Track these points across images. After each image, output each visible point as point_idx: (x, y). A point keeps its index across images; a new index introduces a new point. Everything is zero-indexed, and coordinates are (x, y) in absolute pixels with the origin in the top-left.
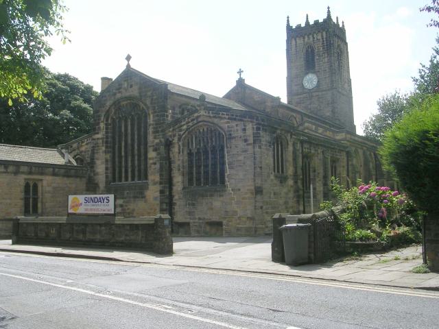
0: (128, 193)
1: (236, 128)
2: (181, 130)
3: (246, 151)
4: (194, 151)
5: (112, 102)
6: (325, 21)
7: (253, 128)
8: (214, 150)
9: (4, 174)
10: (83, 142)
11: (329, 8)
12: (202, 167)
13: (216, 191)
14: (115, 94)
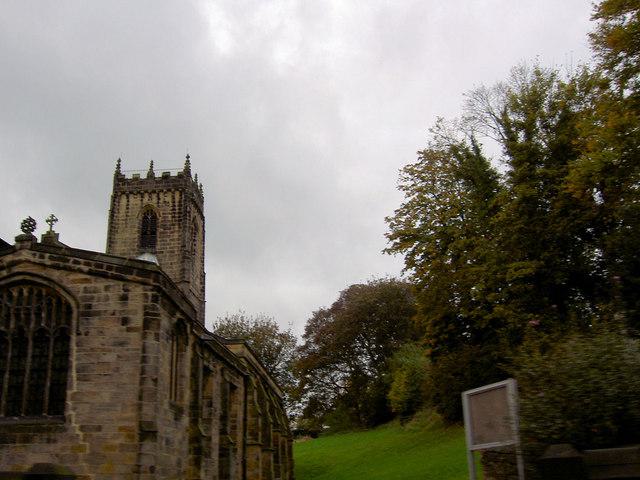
1: (104, 293)
6: (180, 176)
8: (41, 337)
11: (188, 157)
12: (7, 376)
13: (39, 430)
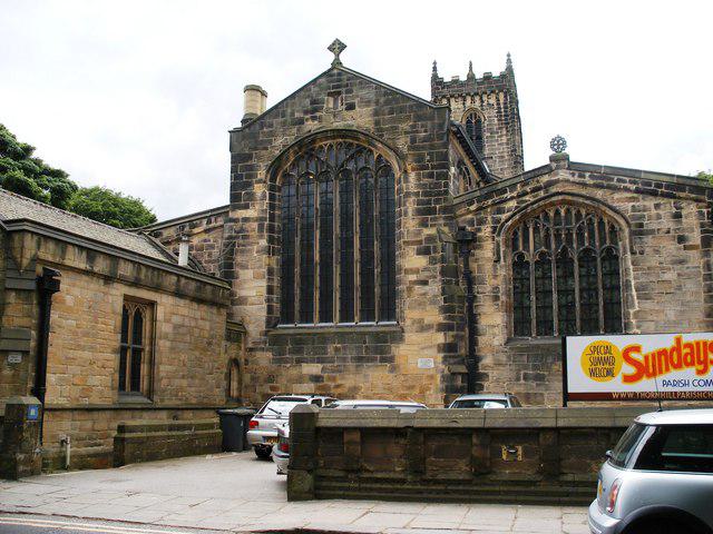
0: (337, 349)
1: (654, 212)
2: (500, 211)
3: (681, 262)
4: (531, 257)
5: (291, 140)
6: (503, 76)
7: (701, 213)
9: (85, 278)
10: (195, 226)
14: (301, 122)
